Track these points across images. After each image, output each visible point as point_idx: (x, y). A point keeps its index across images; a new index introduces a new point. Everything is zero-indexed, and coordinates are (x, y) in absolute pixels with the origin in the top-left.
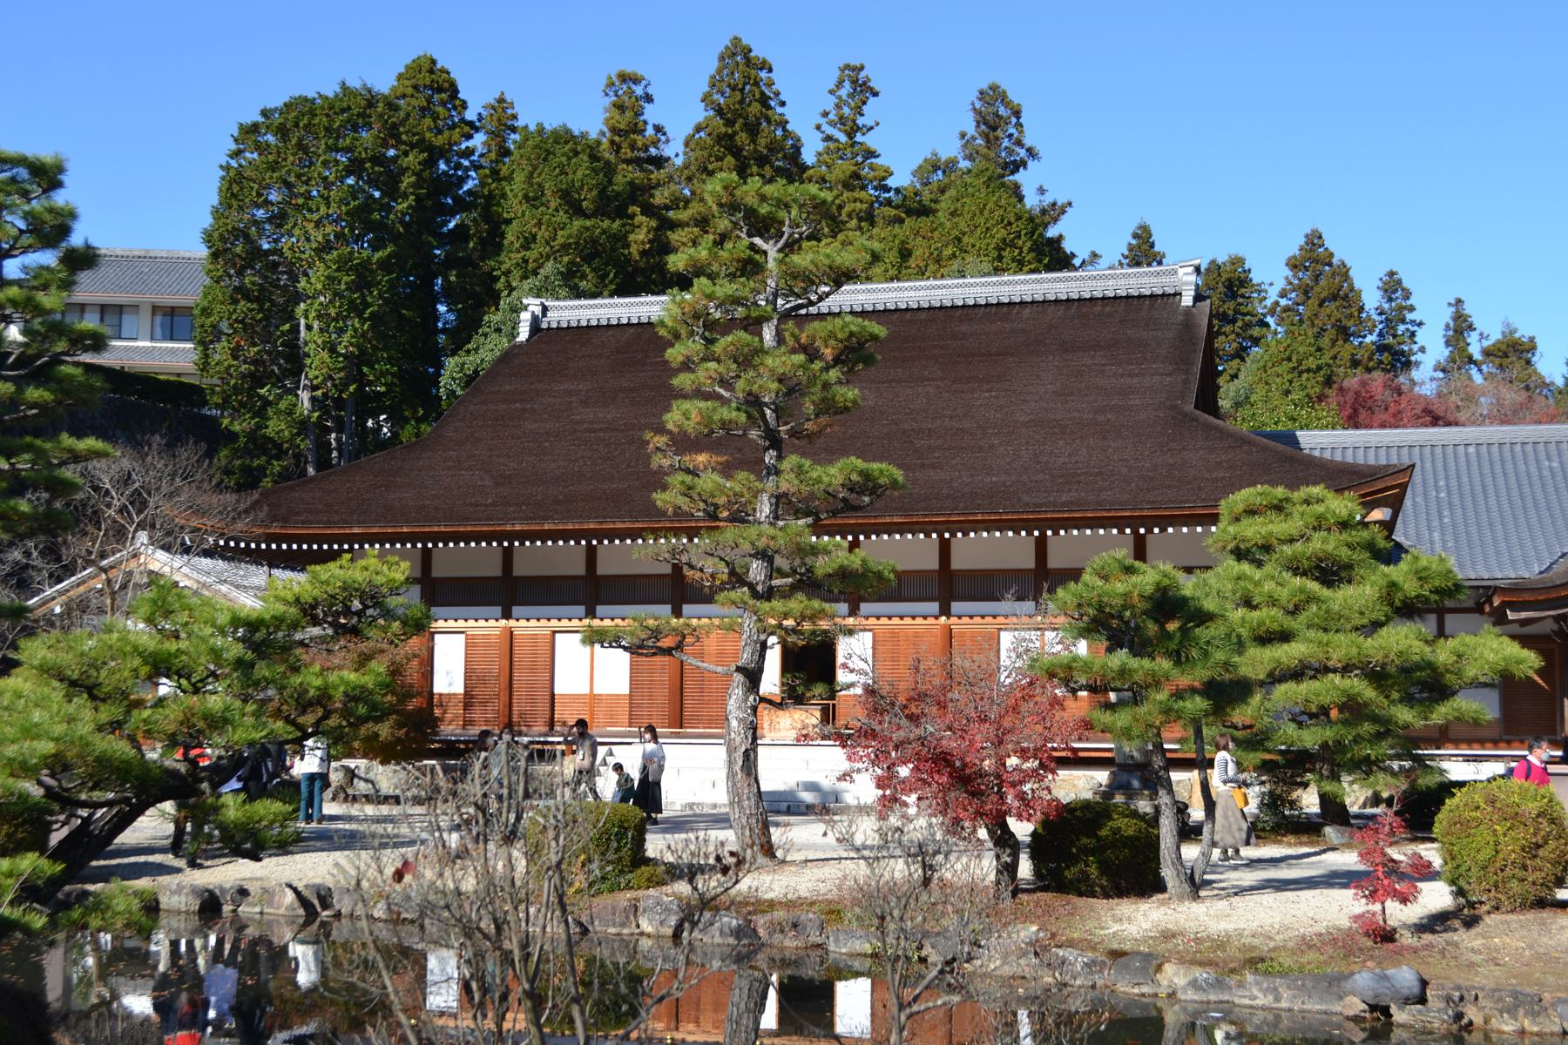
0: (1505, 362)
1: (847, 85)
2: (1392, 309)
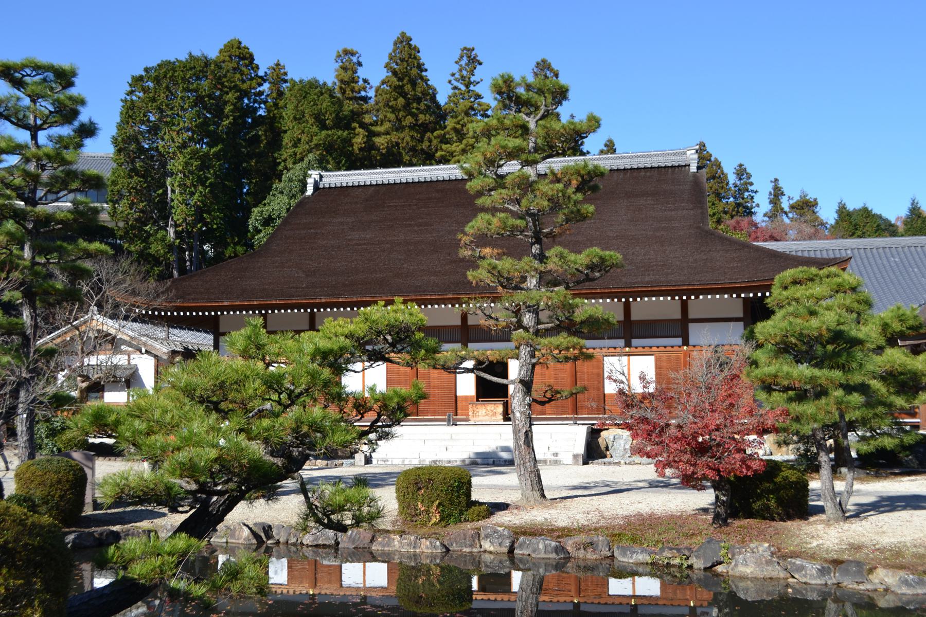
0: (802, 211)
1: (465, 58)
2: (741, 184)
